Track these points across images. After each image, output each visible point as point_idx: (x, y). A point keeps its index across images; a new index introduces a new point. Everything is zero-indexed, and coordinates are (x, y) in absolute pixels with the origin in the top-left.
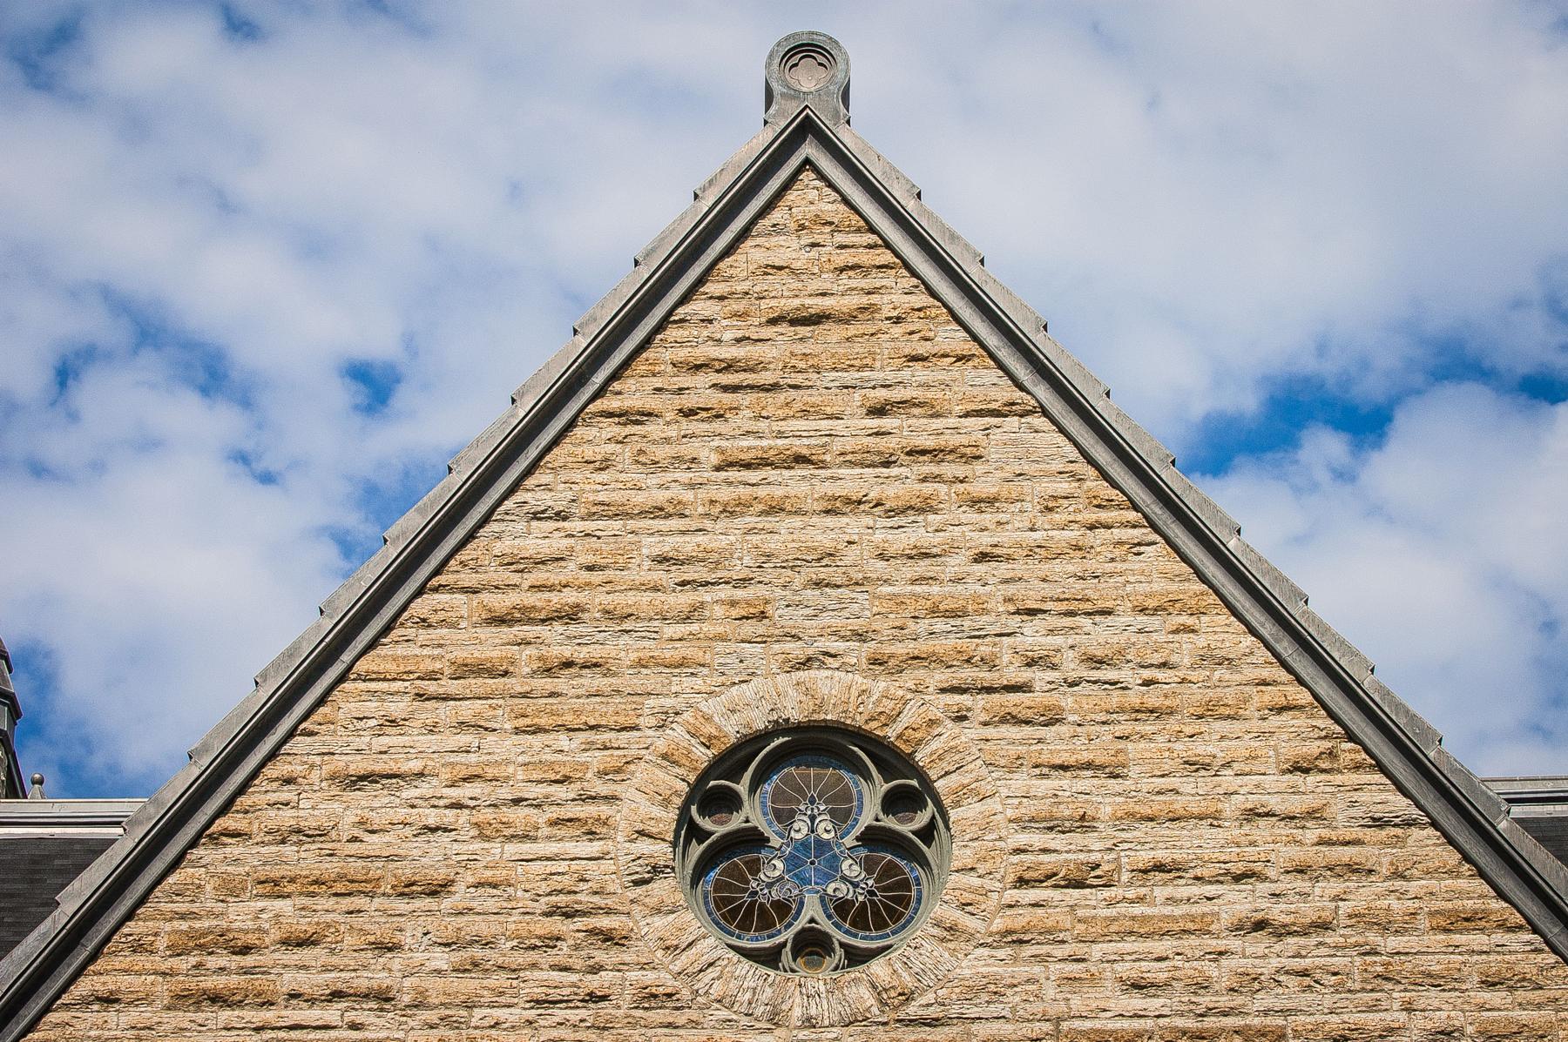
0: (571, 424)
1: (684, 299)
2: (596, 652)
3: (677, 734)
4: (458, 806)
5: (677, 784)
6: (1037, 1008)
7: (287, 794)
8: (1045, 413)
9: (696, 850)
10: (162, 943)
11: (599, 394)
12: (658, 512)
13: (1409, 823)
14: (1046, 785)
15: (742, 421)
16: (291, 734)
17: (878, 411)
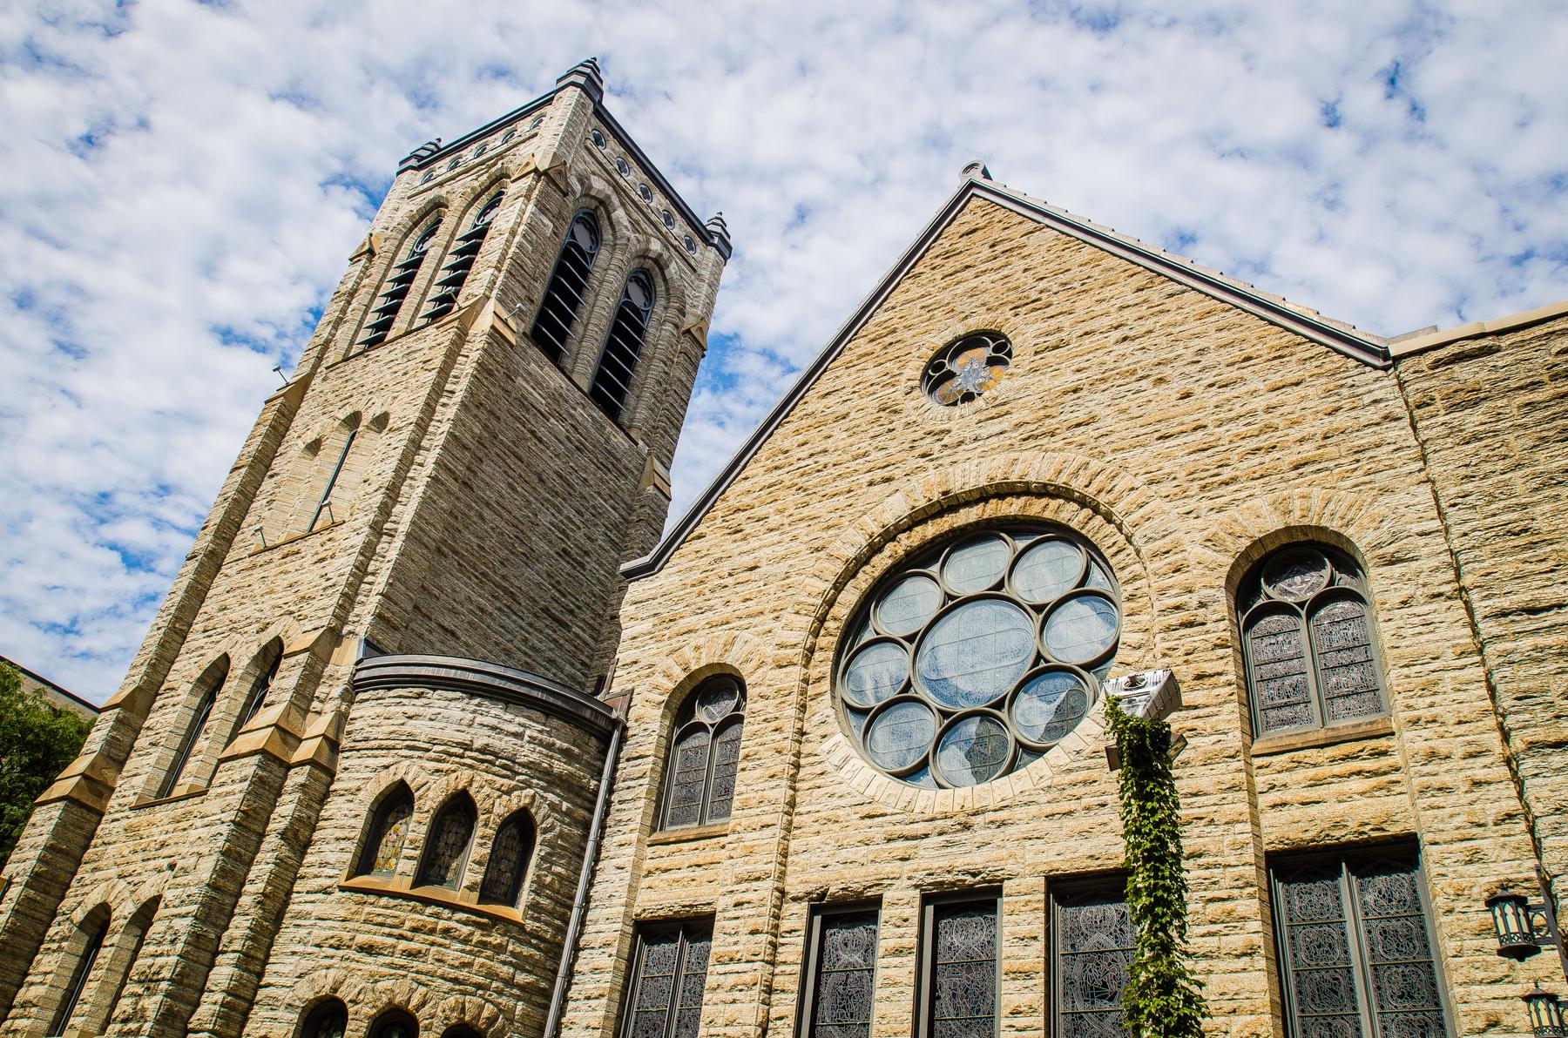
5: (922, 364)
11: (908, 273)
13: (1183, 292)
17: (993, 246)
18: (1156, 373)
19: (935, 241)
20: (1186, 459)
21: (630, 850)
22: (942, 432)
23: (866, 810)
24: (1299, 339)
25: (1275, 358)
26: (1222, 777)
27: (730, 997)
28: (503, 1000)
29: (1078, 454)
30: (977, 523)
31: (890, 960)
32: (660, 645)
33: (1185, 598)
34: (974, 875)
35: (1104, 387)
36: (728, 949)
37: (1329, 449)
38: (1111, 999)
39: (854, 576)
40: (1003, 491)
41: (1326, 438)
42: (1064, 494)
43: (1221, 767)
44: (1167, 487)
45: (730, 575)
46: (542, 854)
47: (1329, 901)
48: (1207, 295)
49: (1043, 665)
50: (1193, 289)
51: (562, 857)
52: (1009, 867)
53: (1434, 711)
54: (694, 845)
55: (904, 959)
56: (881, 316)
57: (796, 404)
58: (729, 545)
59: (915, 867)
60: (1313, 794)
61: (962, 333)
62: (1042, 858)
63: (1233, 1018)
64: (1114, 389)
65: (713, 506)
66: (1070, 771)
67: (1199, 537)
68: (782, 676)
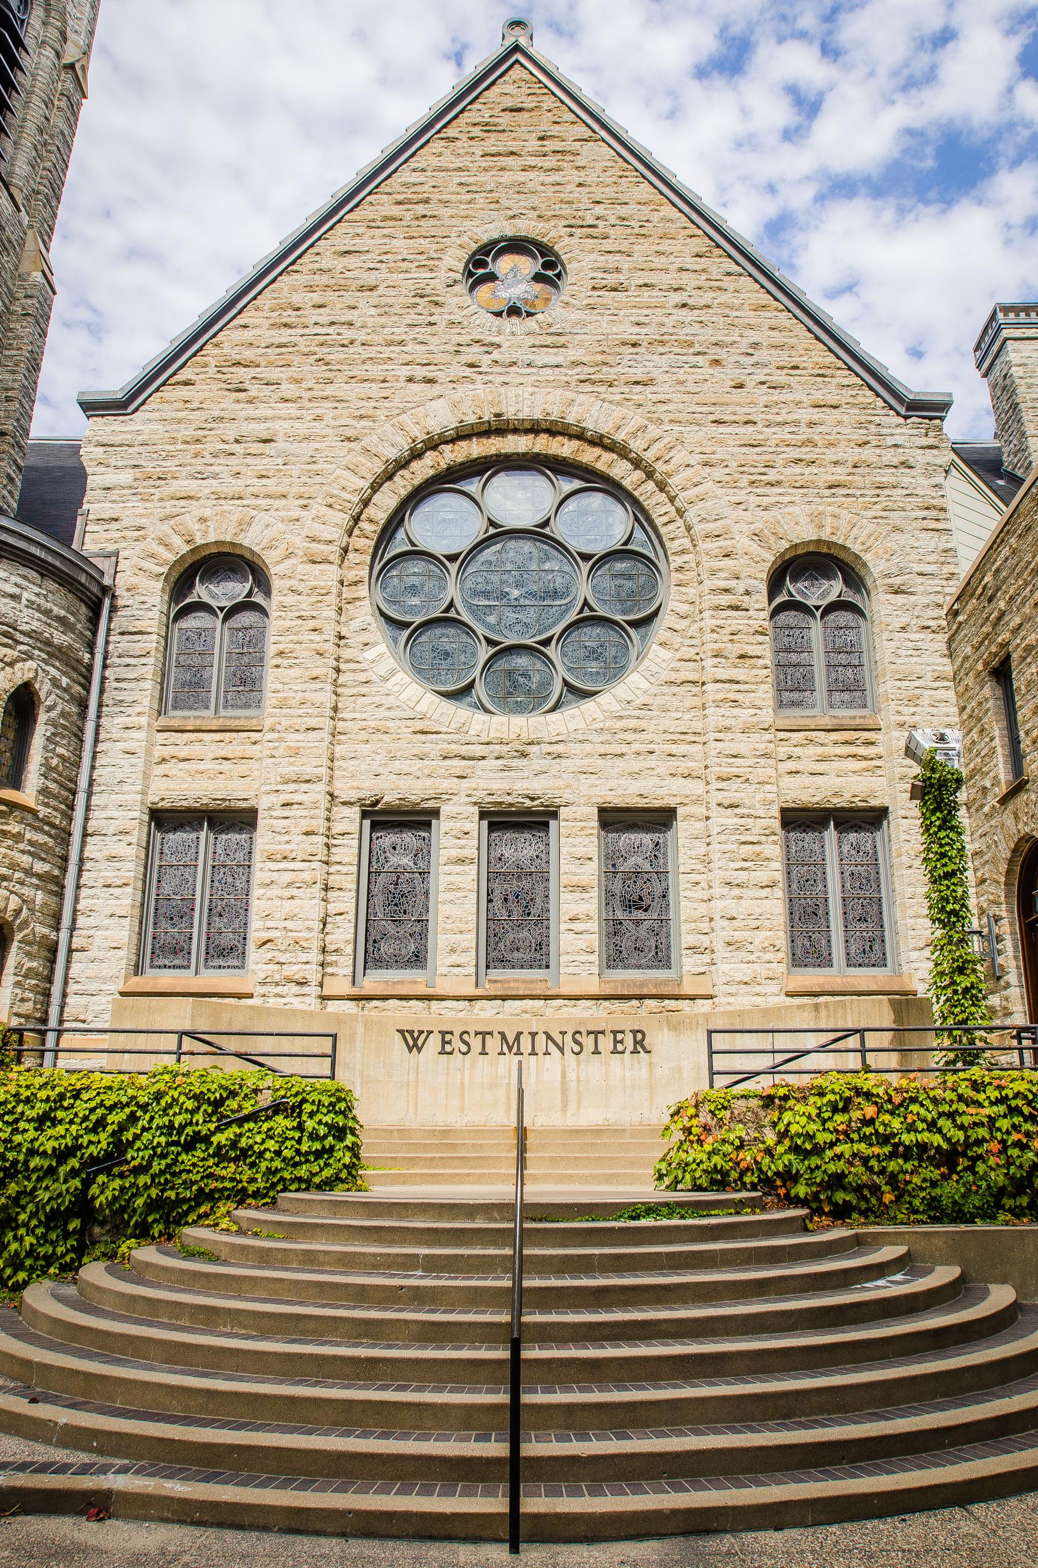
0: (428, 142)
1: (471, 103)
2: (435, 213)
3: (465, 239)
4: (381, 262)
6: (600, 331)
7: (317, 258)
8: (603, 140)
9: (471, 280)
10: (266, 308)
11: (438, 132)
12: (460, 169)
13: (740, 275)
14: (603, 258)
15: (492, 141)
16: (319, 239)
17: (542, 139)
18: (714, 353)
19: (471, 103)
20: (737, 450)
21: (141, 735)
22: (492, 345)
23: (419, 725)
24: (840, 364)
25: (819, 375)
26: (757, 746)
27: (288, 893)
28: (25, 891)
29: (635, 414)
30: (524, 454)
31: (452, 867)
32: (148, 505)
33: (732, 583)
34: (532, 799)
35: (661, 350)
36: (280, 847)
37: (857, 478)
38: (646, 910)
39: (390, 478)
40: (554, 430)
41: (855, 467)
42: (621, 450)
43: (756, 737)
44: (718, 473)
45: (237, 441)
46: (48, 734)
47: (816, 847)
48: (763, 287)
49: (587, 613)
50: (750, 275)
51: (63, 737)
52: (566, 796)
53: (915, 719)
54: (218, 736)
55: (467, 868)
56: (405, 175)
57: (305, 252)
58: (229, 403)
59: (474, 785)
60: (820, 767)
61: (510, 234)
62: (596, 791)
63: (756, 932)
64: (671, 356)
65: (201, 349)
66: (621, 717)
67: (745, 528)
68: (317, 572)
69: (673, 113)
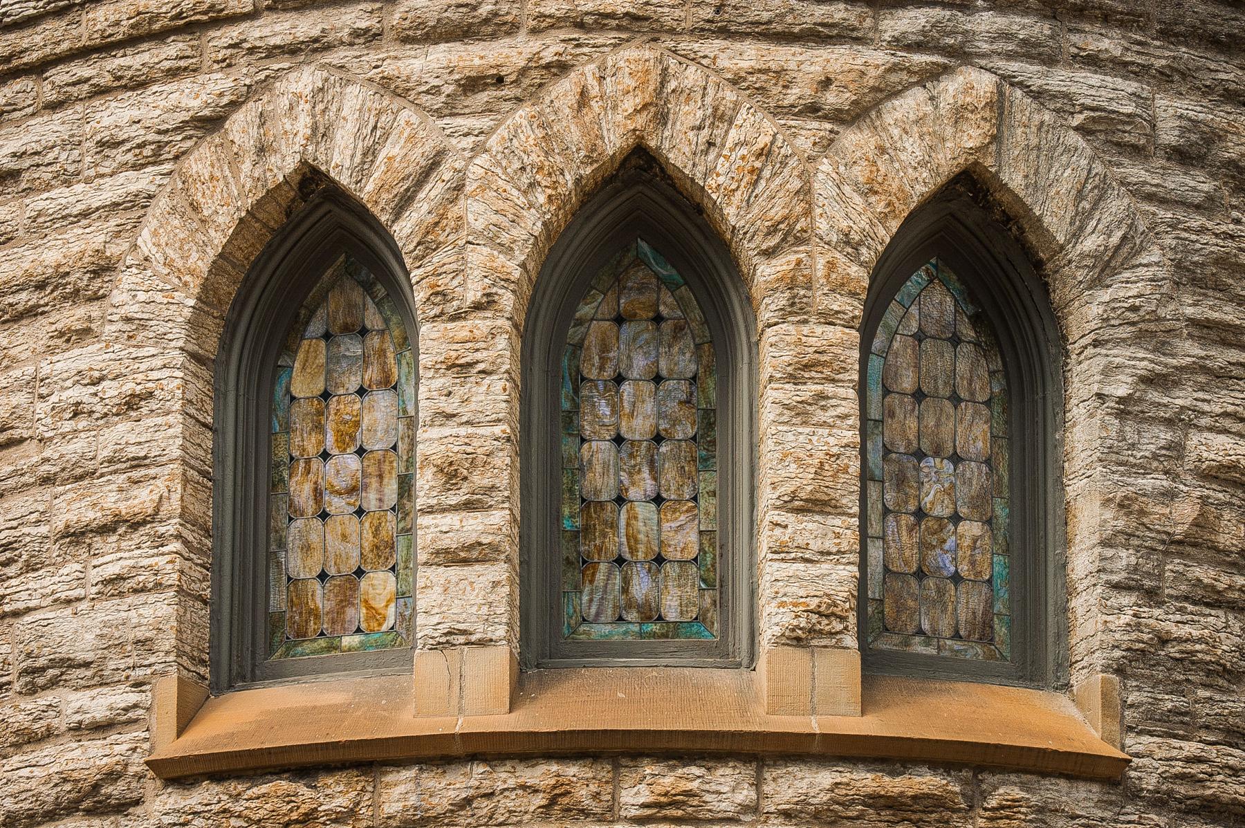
69: (406, 339)
